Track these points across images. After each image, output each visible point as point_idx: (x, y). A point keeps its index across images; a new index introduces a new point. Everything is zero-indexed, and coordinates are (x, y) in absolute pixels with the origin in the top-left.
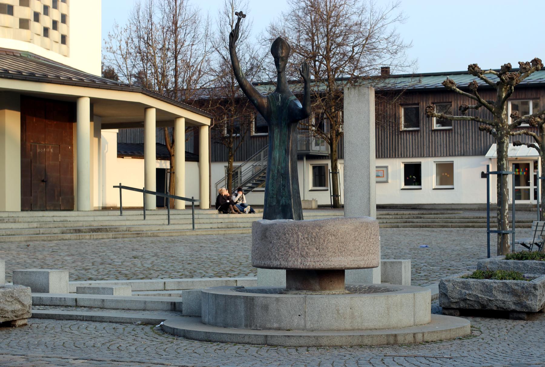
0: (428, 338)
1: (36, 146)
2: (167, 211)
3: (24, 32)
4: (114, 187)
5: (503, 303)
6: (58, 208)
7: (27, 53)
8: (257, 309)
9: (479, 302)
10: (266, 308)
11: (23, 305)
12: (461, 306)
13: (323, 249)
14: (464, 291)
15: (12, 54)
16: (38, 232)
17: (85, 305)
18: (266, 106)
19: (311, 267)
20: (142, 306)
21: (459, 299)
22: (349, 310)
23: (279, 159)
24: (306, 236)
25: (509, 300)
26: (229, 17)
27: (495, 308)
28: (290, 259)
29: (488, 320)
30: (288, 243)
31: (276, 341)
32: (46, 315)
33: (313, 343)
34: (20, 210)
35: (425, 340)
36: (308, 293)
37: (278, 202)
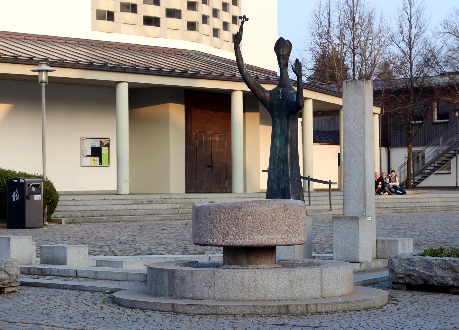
0: (320, 309)
1: (202, 135)
2: (329, 193)
3: (192, 33)
4: (263, 171)
5: (443, 279)
6: (224, 191)
7: (196, 52)
8: (177, 280)
9: (421, 278)
10: (183, 280)
11: (9, 275)
12: (407, 280)
13: (242, 228)
14: (408, 267)
15: (180, 53)
16: (177, 212)
17: (83, 276)
18: (268, 99)
19: (231, 244)
20: (124, 277)
21: (404, 274)
22: (253, 282)
23: (280, 147)
24: (227, 216)
25: (448, 276)
26: (407, 13)
27: (436, 284)
28: (214, 237)
29: (441, 295)
30: (213, 222)
31: (181, 309)
32: (42, 283)
33: (211, 311)
34: (185, 193)
35: (319, 311)
36: (236, 267)
37: (278, 185)
